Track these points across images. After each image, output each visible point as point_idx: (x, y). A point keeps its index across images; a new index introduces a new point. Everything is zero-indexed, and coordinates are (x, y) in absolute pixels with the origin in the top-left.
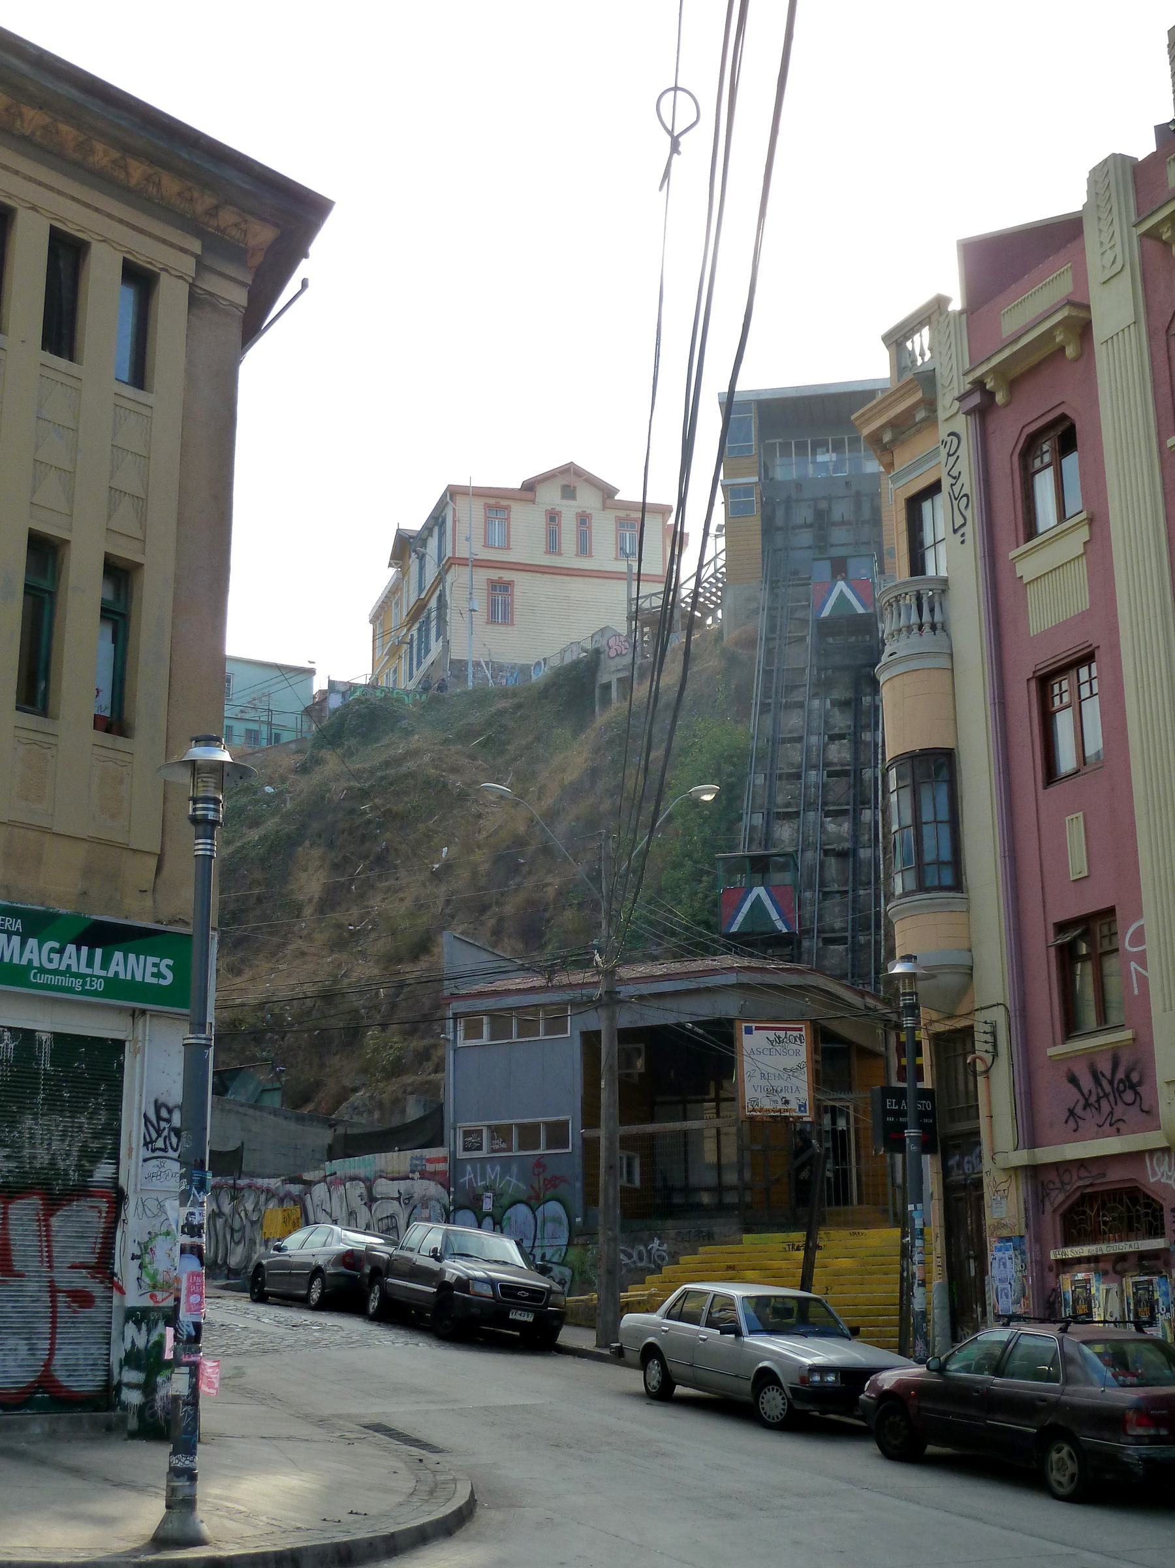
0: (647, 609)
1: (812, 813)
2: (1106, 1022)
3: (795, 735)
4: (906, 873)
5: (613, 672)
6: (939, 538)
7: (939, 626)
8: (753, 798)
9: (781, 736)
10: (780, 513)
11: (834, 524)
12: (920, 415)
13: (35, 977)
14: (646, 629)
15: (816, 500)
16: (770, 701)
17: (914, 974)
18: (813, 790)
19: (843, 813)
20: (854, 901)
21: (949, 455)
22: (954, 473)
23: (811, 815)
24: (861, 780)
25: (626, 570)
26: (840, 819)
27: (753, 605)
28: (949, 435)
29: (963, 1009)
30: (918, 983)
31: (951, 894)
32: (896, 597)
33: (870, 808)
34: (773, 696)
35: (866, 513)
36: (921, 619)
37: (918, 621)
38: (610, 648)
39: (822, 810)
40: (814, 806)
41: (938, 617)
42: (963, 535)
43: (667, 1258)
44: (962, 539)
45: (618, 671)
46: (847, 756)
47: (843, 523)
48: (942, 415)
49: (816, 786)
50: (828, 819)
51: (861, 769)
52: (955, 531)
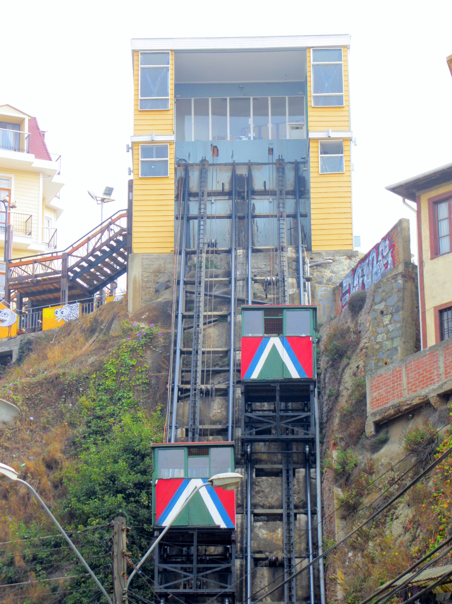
3: (219, 427)
10: (194, 176)
11: (254, 193)
15: (234, 165)
16: (188, 386)
19: (279, 517)
39: (252, 513)
43: (129, 361)
47: (265, 193)
50: (259, 524)
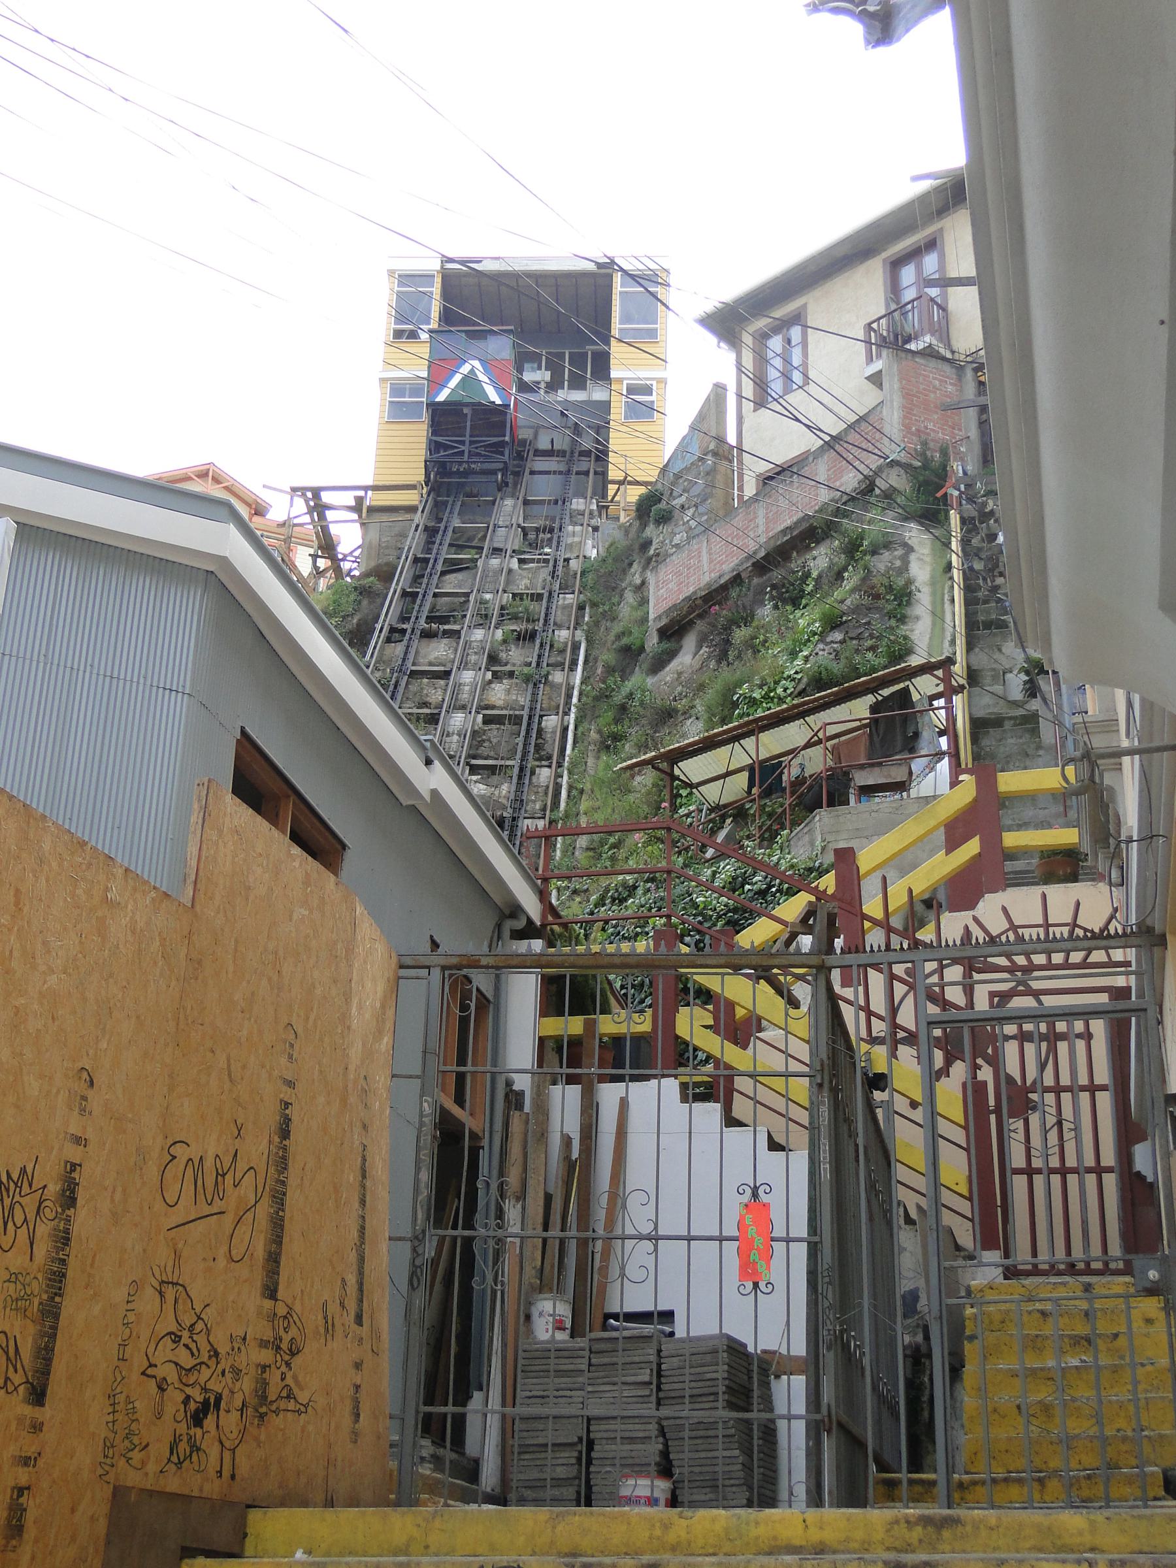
2: (611, 1231)
13: (426, 1101)
18: (455, 738)
24: (540, 731)
26: (495, 779)
33: (550, 767)
46: (683, 1014)
49: (461, 734)
51: (541, 716)
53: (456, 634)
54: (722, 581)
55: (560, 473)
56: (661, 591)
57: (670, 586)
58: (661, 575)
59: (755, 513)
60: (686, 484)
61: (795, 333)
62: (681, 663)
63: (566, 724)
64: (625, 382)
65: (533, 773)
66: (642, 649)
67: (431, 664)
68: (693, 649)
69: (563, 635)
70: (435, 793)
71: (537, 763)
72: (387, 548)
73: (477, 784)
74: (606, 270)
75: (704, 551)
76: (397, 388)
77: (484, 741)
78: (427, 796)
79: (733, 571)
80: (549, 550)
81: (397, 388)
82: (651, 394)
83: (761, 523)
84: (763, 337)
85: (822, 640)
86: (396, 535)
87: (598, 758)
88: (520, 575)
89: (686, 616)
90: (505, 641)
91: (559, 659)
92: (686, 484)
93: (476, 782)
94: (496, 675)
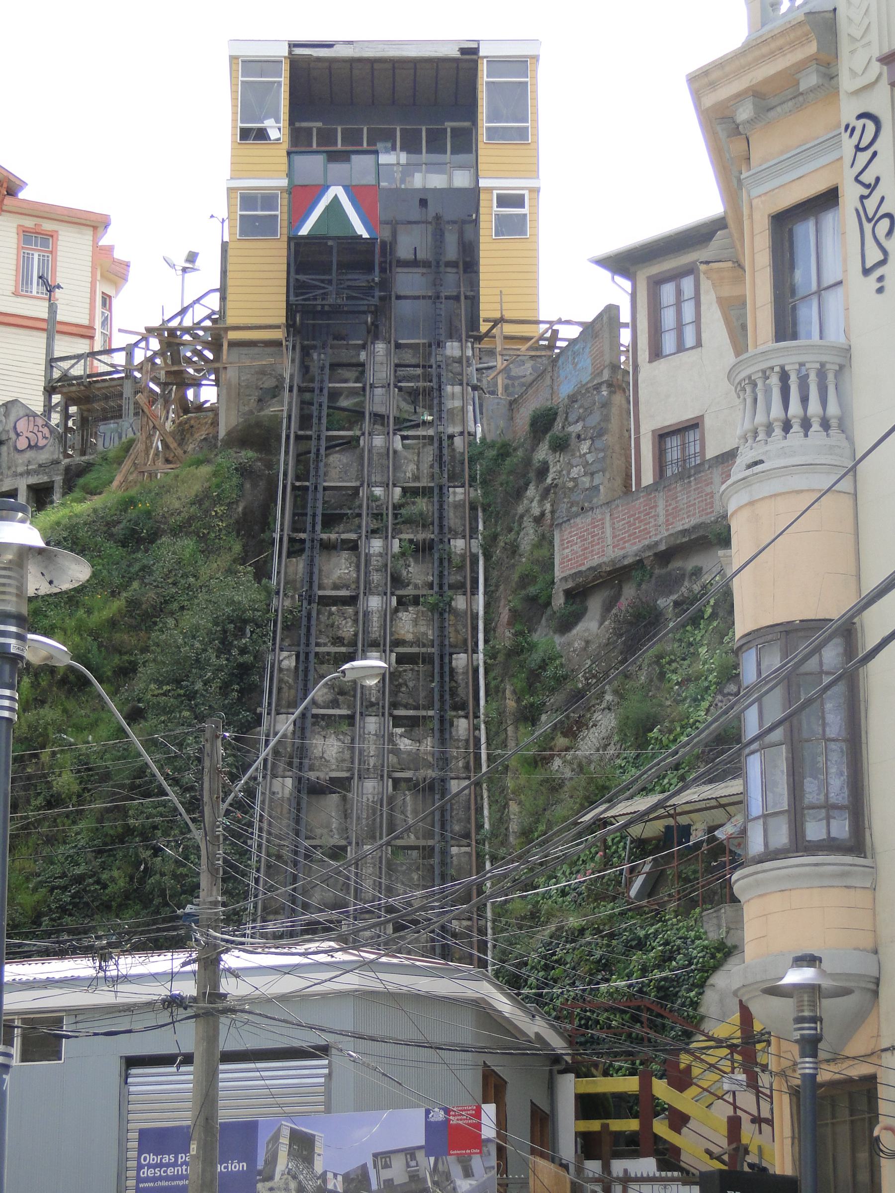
0: (80, 377)
1: (372, 719)
4: (772, 821)
5: (21, 475)
6: (828, 280)
7: (834, 423)
8: (280, 690)
9: (321, 593)
12: (810, 80)
14: (73, 409)
16: (302, 536)
17: (819, 986)
20: (443, 863)
21: (858, 149)
22: (868, 178)
23: (372, 724)
24: (452, 671)
25: (45, 315)
27: (269, 383)
28: (860, 116)
29: (858, 1046)
30: (823, 1000)
31: (848, 859)
32: (764, 372)
34: (309, 528)
35: (452, 252)
36: (769, 415)
37: (782, 415)
38: (18, 435)
40: (374, 708)
41: (833, 409)
42: (881, 279)
44: (879, 285)
45: (28, 473)
48: (847, 83)
50: (399, 731)
51: (451, 654)
52: (866, 272)
53: (353, 546)
54: (626, 562)
55: (430, 297)
56: (567, 551)
57: (574, 547)
58: (566, 535)
59: (655, 502)
60: (581, 411)
61: (687, 283)
62: (587, 630)
63: (475, 663)
64: (495, 192)
65: (452, 725)
66: (548, 604)
67: (336, 587)
68: (598, 617)
69: (458, 545)
70: (537, 1034)
71: (453, 713)
72: (247, 387)
73: (403, 739)
74: (470, 53)
75: (608, 524)
76: (248, 200)
77: (400, 685)
78: (533, 1036)
79: (636, 555)
80: (430, 418)
81: (248, 200)
82: (523, 206)
83: (661, 514)
84: (656, 283)
85: (720, 691)
86: (257, 373)
87: (517, 728)
88: (406, 458)
89: (590, 583)
90: (403, 554)
91: (459, 578)
92: (581, 411)
93: (401, 736)
94: (402, 603)
